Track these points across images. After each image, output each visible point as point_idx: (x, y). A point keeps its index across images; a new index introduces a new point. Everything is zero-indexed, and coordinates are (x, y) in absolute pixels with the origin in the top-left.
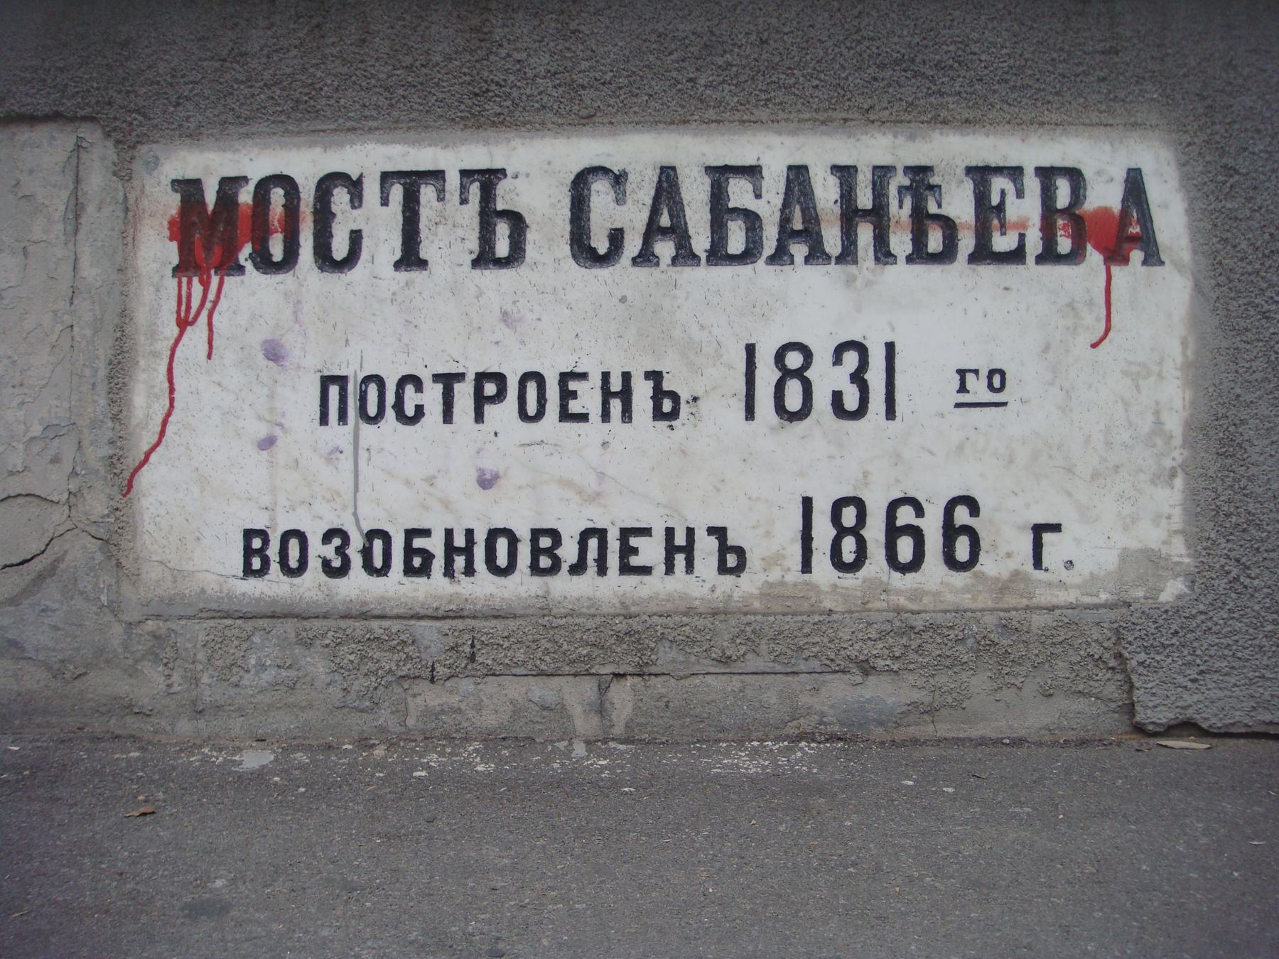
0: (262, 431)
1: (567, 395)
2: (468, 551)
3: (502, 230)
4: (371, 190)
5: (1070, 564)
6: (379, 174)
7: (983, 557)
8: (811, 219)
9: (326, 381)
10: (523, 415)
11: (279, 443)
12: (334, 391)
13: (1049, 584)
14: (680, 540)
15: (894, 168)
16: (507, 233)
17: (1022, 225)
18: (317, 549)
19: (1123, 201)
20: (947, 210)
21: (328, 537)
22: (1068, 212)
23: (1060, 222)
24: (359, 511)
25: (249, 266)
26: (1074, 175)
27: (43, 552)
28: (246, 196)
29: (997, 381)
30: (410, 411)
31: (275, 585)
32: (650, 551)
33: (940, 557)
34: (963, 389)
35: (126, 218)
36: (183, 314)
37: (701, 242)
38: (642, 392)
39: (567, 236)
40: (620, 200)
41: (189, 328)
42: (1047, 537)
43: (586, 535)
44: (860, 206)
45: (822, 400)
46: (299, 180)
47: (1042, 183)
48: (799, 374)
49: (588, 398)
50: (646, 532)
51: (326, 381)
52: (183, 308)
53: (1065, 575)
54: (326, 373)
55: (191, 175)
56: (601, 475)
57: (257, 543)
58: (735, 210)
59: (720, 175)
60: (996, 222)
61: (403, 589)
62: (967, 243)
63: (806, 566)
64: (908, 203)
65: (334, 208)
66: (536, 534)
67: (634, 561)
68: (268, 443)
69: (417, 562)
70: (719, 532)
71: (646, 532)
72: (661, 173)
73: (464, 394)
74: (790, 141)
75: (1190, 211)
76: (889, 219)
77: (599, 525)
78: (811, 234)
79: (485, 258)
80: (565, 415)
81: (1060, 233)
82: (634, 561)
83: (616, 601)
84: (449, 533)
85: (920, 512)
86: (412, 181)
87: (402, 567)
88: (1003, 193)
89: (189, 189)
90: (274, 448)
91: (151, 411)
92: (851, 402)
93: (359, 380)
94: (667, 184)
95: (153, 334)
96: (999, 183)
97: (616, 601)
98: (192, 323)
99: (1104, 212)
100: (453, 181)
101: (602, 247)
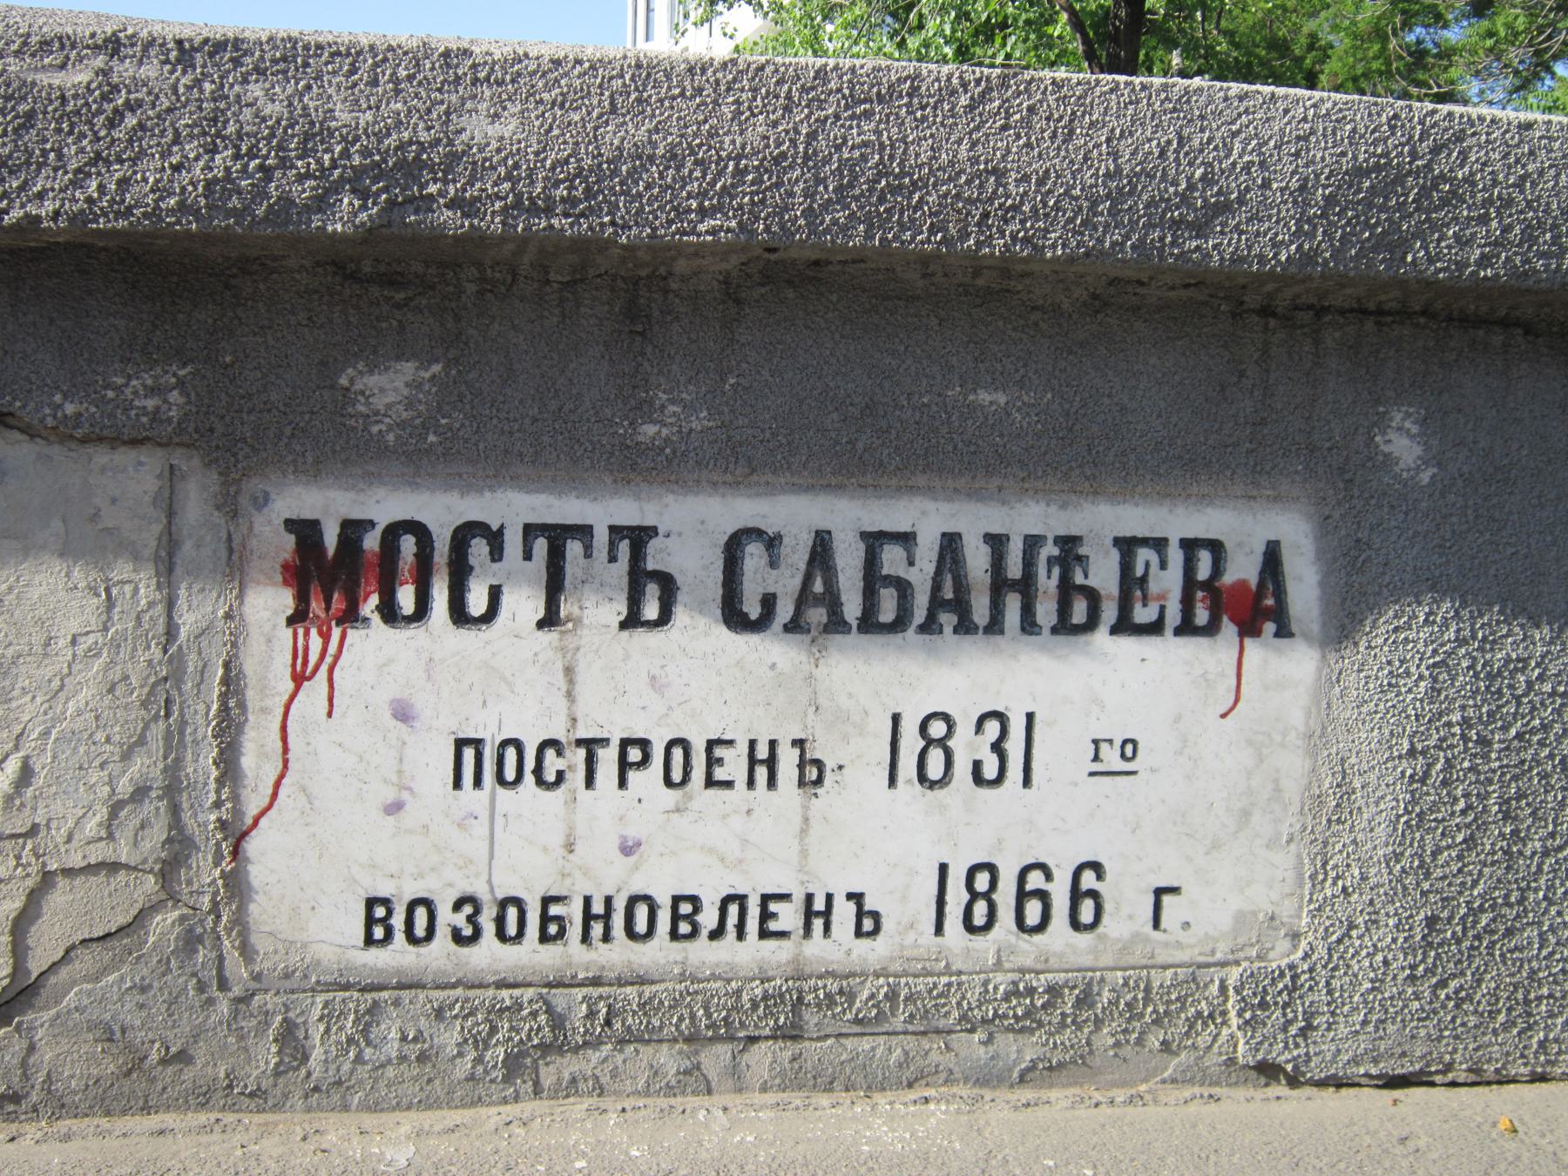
0: (390, 795)
1: (712, 762)
2: (607, 916)
3: (652, 590)
4: (513, 542)
5: (1186, 925)
6: (521, 526)
7: (1105, 920)
8: (961, 587)
9: (460, 744)
10: (668, 782)
11: (407, 808)
12: (469, 754)
13: (1166, 945)
14: (819, 905)
15: (1045, 537)
16: (658, 594)
17: (1162, 597)
18: (447, 917)
19: (1261, 573)
20: (1092, 582)
21: (457, 906)
22: (1209, 586)
23: (1200, 594)
24: (493, 879)
25: (376, 619)
26: (1216, 547)
27: (130, 924)
28: (371, 542)
29: (1129, 749)
30: (550, 777)
31: (398, 956)
32: (788, 916)
33: (1066, 920)
34: (1096, 758)
35: (230, 558)
36: (299, 668)
37: (852, 609)
38: (788, 760)
39: (719, 600)
40: (773, 564)
41: (306, 684)
42: (1167, 900)
43: (726, 901)
44: (1010, 576)
45: (962, 768)
46: (433, 527)
47: (1185, 554)
48: (942, 742)
49: (734, 765)
50: (784, 897)
51: (460, 744)
52: (299, 661)
53: (1184, 937)
54: (462, 736)
55: (307, 514)
56: (745, 842)
57: (380, 912)
58: (887, 577)
59: (874, 541)
60: (1138, 593)
61: (537, 958)
62: (1109, 613)
63: (939, 929)
64: (1056, 571)
65: (472, 561)
66: (677, 900)
67: (773, 926)
68: (394, 808)
69: (553, 929)
70: (856, 897)
71: (784, 897)
72: (816, 537)
73: (608, 759)
74: (945, 507)
75: (1322, 584)
76: (1037, 590)
77: (740, 891)
78: (961, 606)
79: (632, 621)
80: (710, 782)
81: (1199, 605)
82: (773, 926)
83: (754, 965)
84: (587, 901)
85: (1049, 876)
86: (558, 536)
87: (537, 935)
88: (1147, 565)
89: (305, 532)
90: (402, 813)
91: (261, 772)
92: (990, 771)
93: (497, 744)
94: (821, 551)
95: (263, 690)
96: (1144, 555)
97: (754, 965)
98: (309, 679)
99: (1242, 584)
100: (601, 537)
101: (753, 610)
